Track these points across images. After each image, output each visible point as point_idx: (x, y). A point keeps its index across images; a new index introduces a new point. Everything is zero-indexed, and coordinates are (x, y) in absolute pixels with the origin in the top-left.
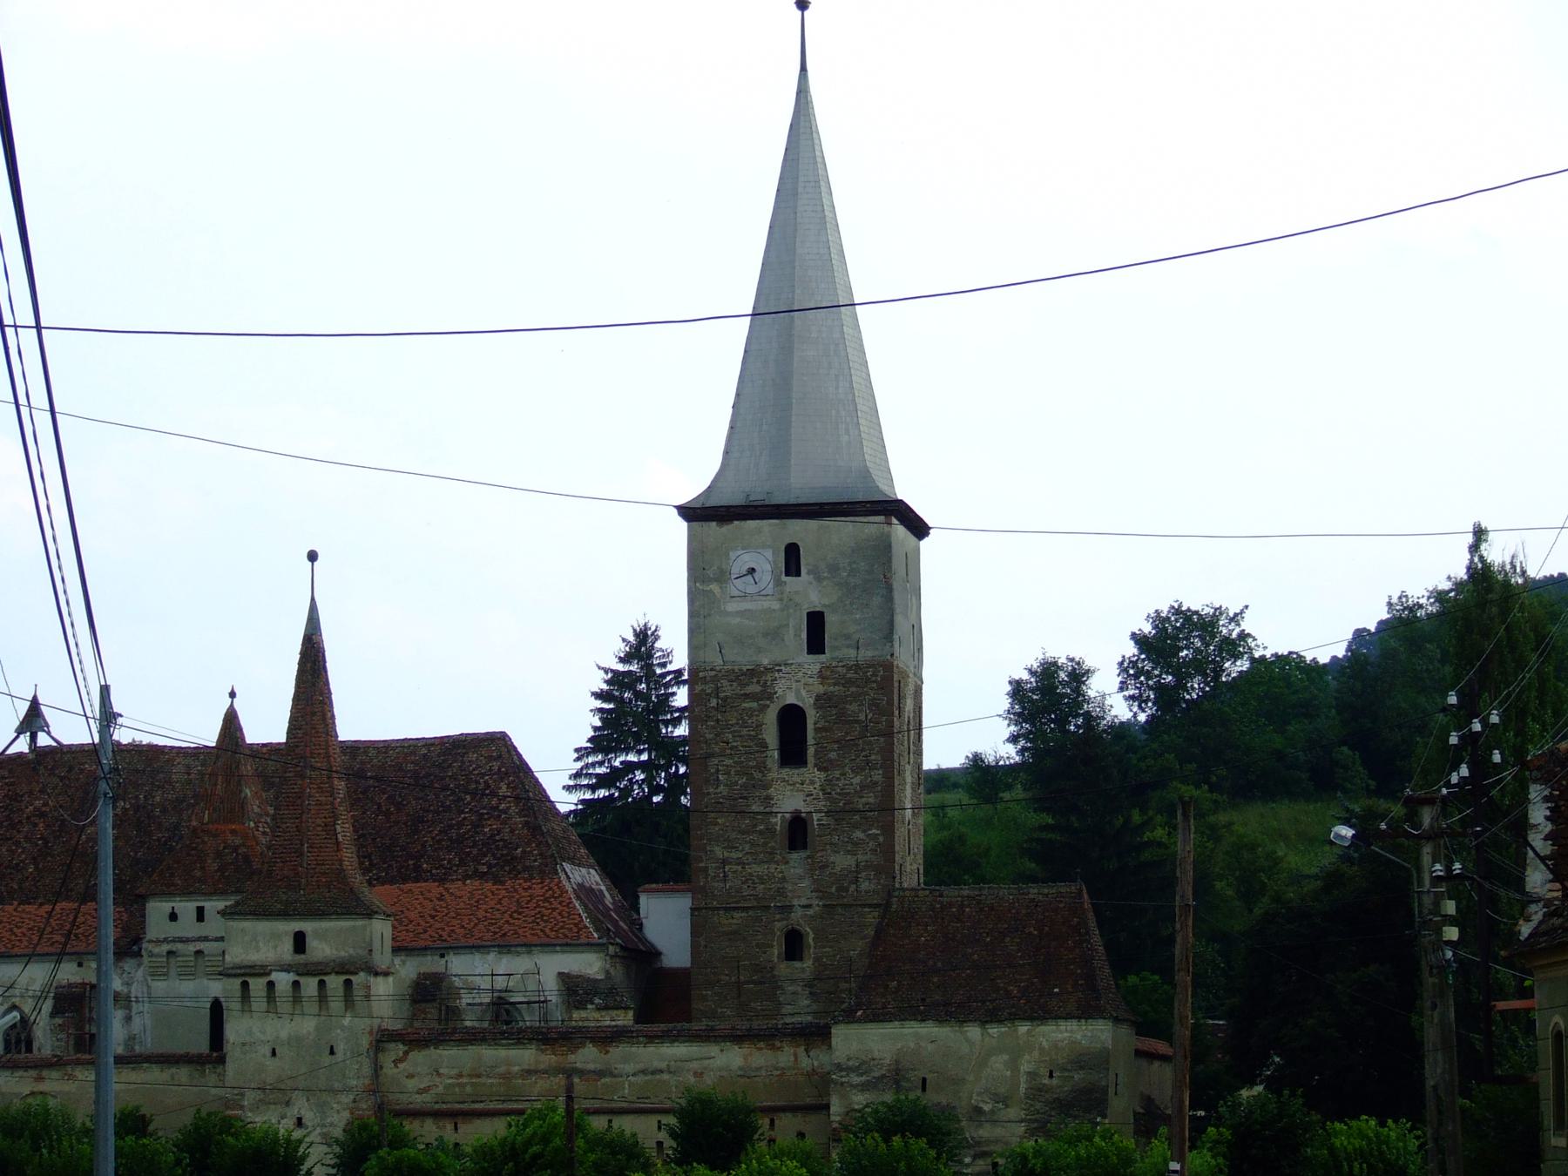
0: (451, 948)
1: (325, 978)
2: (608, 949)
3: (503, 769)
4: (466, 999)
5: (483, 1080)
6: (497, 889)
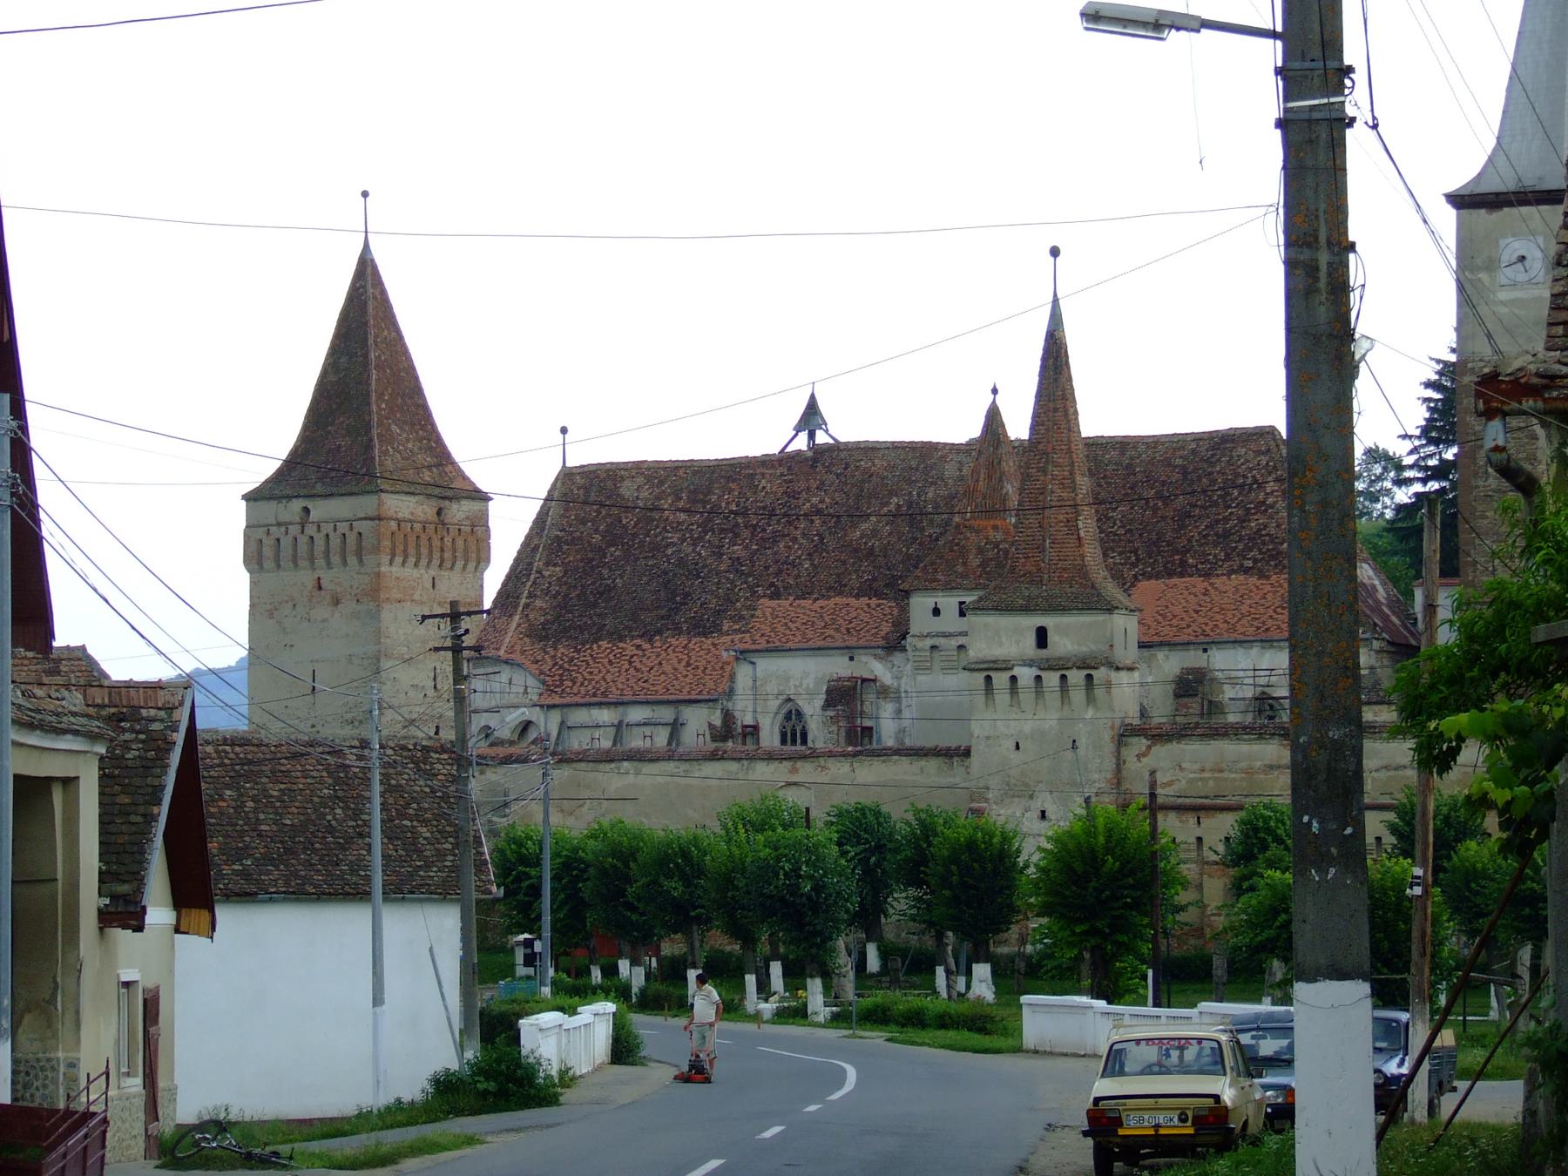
0: (1213, 643)
1: (1092, 672)
2: (1371, 644)
3: (1271, 464)
4: (1229, 692)
5: (1225, 775)
6: (1262, 584)
